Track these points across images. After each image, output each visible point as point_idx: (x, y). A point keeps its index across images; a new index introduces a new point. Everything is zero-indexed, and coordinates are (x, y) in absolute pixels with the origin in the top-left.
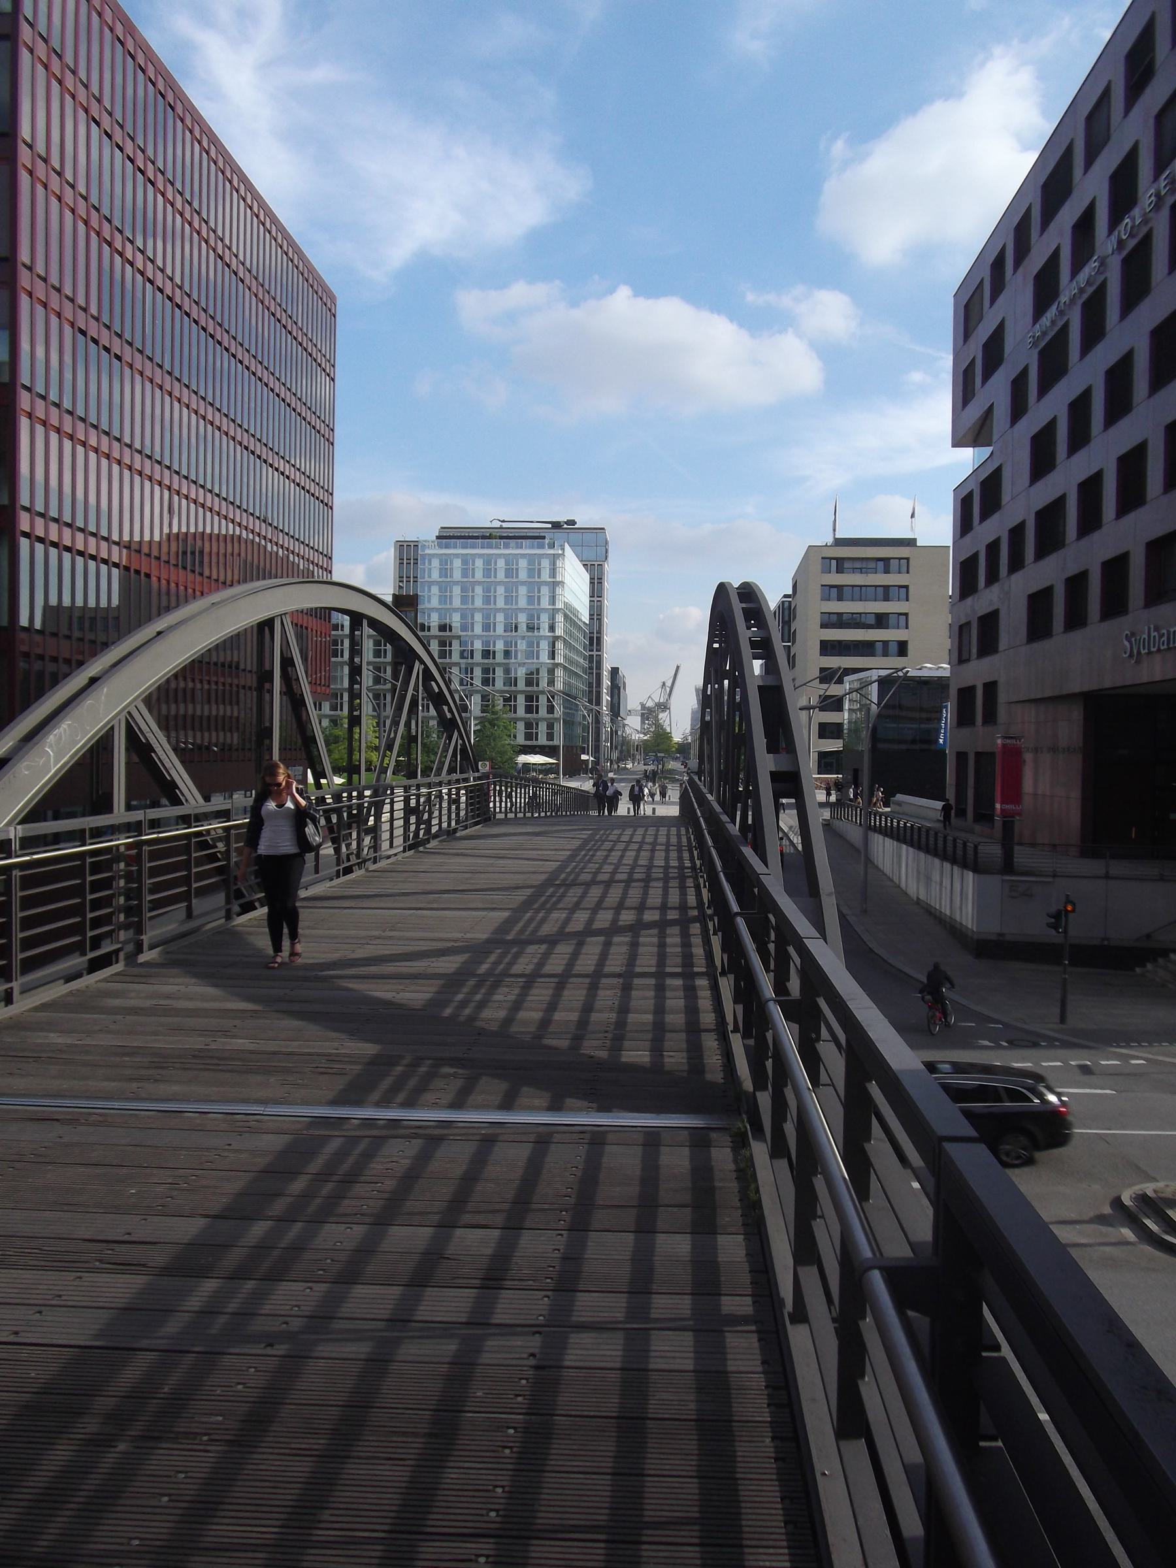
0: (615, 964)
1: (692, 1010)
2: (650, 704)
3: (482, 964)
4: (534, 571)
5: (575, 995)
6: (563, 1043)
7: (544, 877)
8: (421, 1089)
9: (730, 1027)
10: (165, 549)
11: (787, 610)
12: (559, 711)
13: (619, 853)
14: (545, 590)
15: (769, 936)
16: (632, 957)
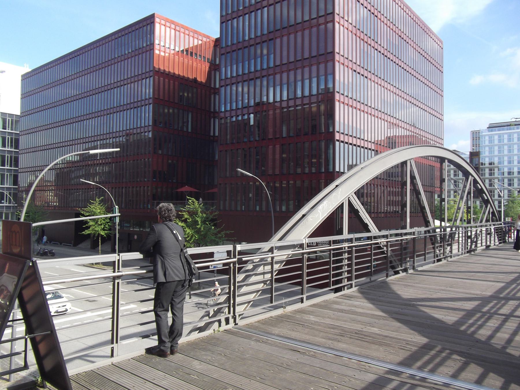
10: (385, 142)
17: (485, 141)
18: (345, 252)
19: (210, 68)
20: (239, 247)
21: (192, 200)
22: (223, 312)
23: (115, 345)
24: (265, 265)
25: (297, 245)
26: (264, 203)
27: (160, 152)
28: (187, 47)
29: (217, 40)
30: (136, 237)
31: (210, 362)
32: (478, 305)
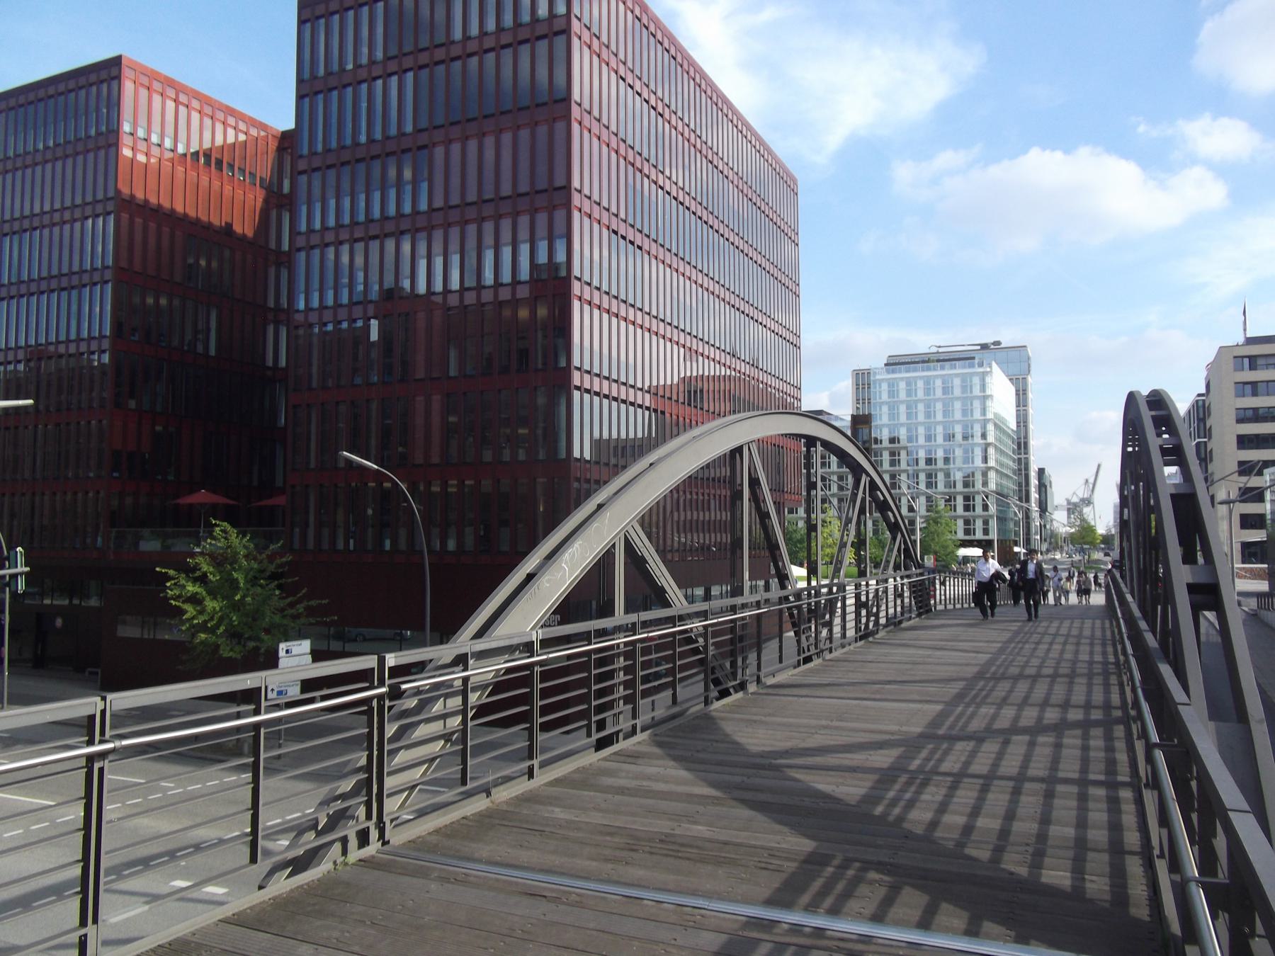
0: (1038, 768)
1: (1115, 827)
2: (1075, 500)
3: (910, 764)
4: (966, 387)
5: (998, 798)
6: (984, 854)
7: (976, 669)
8: (847, 895)
9: (1156, 852)
11: (1201, 410)
12: (993, 509)
13: (1046, 647)
14: (977, 404)
15: (1191, 773)
16: (1055, 762)
17: (881, 393)
18: (619, 655)
19: (266, 201)
20: (391, 660)
21: (221, 527)
22: (352, 817)
23: (90, 930)
24: (447, 696)
25: (519, 645)
26: (403, 533)
27: (132, 404)
28: (207, 145)
29: (285, 136)
30: (59, 622)
31: (341, 945)
32: (899, 757)
